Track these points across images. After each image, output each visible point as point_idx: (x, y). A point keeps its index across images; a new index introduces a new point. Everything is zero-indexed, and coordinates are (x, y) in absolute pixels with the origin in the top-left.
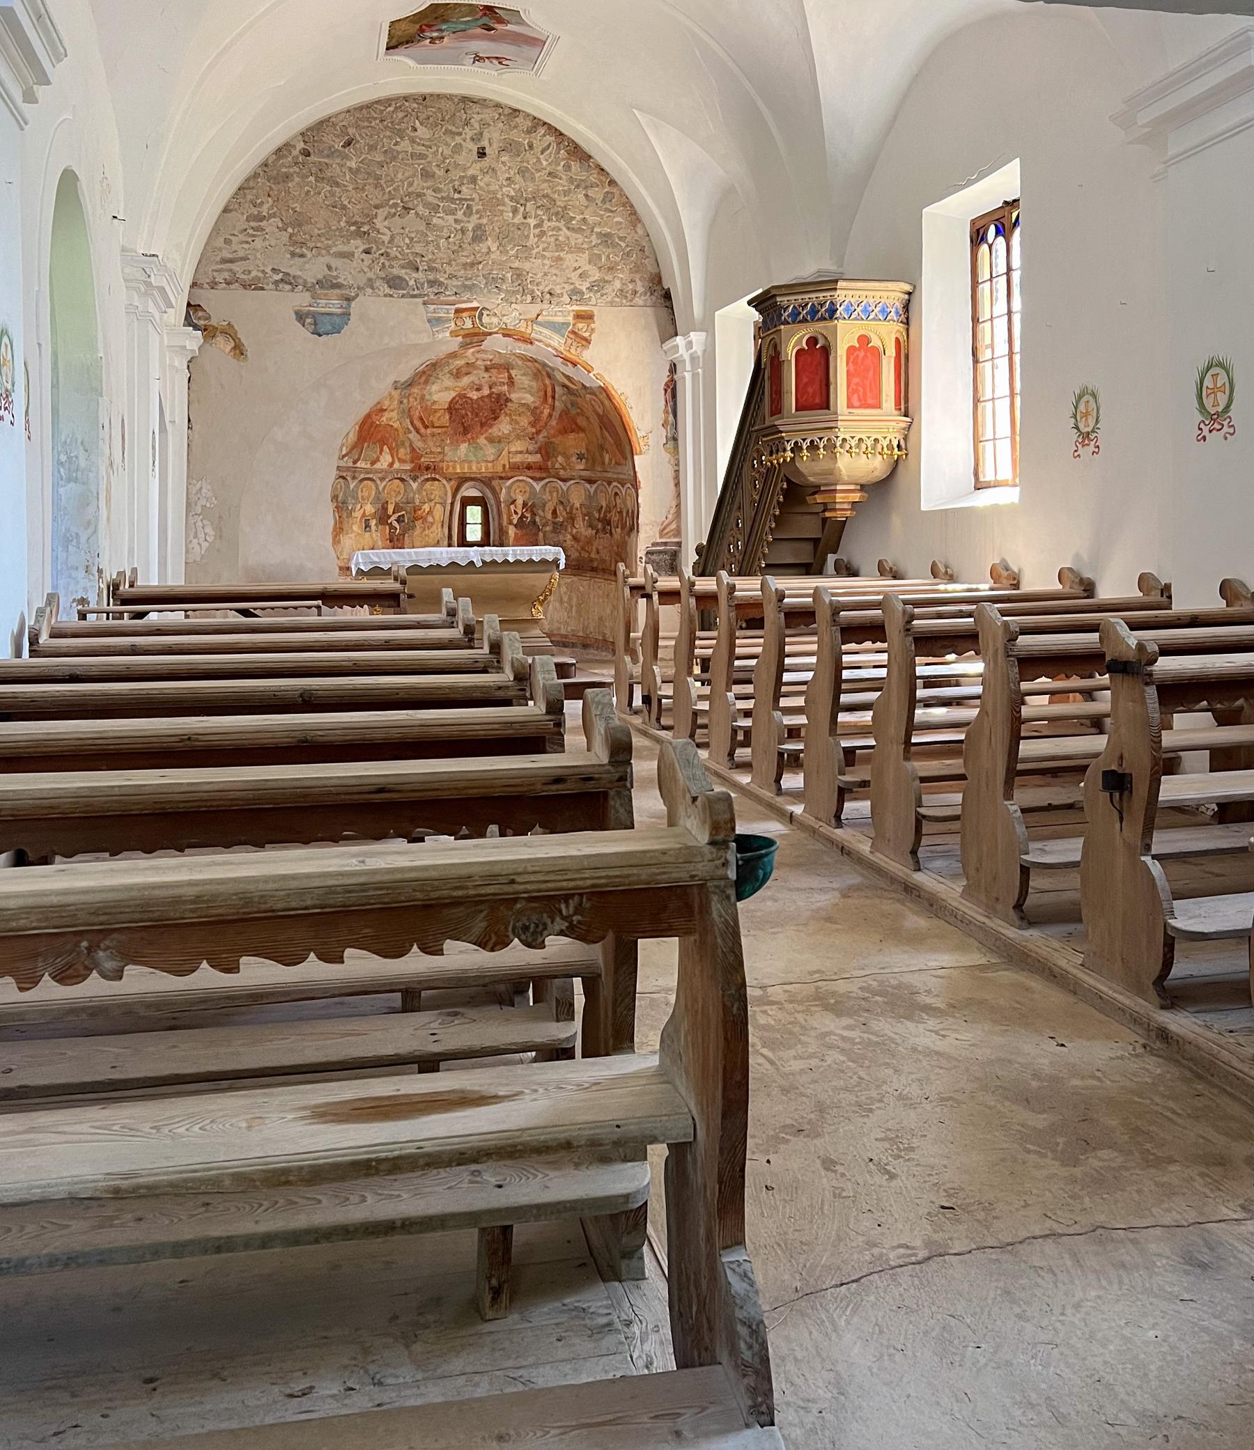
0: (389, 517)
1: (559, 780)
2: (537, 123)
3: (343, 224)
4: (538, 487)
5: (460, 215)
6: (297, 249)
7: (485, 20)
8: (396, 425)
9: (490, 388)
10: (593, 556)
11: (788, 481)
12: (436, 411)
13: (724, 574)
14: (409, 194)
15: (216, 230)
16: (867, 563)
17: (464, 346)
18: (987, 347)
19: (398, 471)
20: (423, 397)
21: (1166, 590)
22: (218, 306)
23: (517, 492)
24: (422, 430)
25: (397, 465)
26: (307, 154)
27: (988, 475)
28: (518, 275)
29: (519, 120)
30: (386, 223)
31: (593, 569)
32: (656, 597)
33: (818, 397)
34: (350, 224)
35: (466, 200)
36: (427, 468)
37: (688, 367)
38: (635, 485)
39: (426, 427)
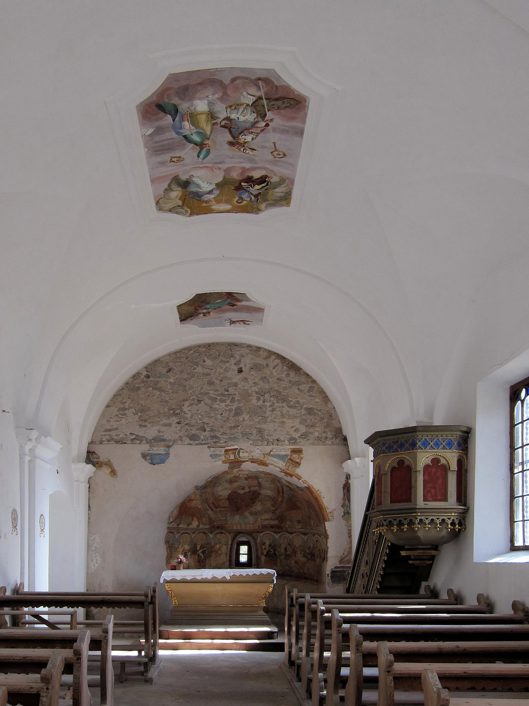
0: (198, 551)
2: (271, 353)
3: (166, 410)
4: (277, 536)
5: (228, 402)
6: (143, 422)
7: (229, 301)
8: (200, 507)
9: (249, 488)
10: (306, 571)
12: (221, 500)
14: (201, 394)
15: (103, 415)
17: (230, 468)
19: (202, 529)
20: (213, 493)
22: (104, 452)
23: (266, 539)
24: (215, 509)
25: (201, 526)
26: (148, 377)
27: (519, 543)
28: (260, 431)
29: (261, 352)
30: (189, 408)
31: (306, 578)
34: (170, 410)
35: (230, 395)
36: (218, 528)
38: (326, 537)
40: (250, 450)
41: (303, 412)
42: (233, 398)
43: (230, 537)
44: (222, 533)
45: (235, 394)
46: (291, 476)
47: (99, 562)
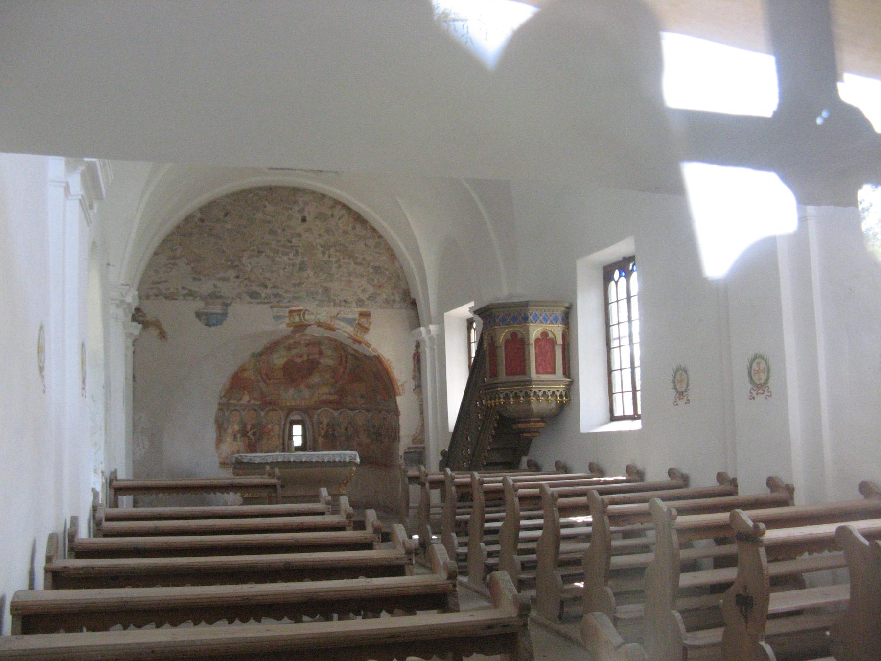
1: (490, 627)
2: (337, 203)
3: (223, 261)
4: (336, 414)
5: (291, 255)
11: (500, 415)
15: (150, 265)
16: (548, 464)
17: (294, 332)
18: (615, 339)
21: (734, 482)
22: (152, 310)
23: (325, 416)
26: (202, 220)
27: (618, 412)
32: (427, 485)
33: (518, 363)
34: (226, 261)
36: (270, 403)
37: (428, 344)
38: (397, 413)
40: (318, 313)
41: (370, 270)
42: (296, 250)
43: (283, 415)
46: (360, 343)
47: (147, 447)
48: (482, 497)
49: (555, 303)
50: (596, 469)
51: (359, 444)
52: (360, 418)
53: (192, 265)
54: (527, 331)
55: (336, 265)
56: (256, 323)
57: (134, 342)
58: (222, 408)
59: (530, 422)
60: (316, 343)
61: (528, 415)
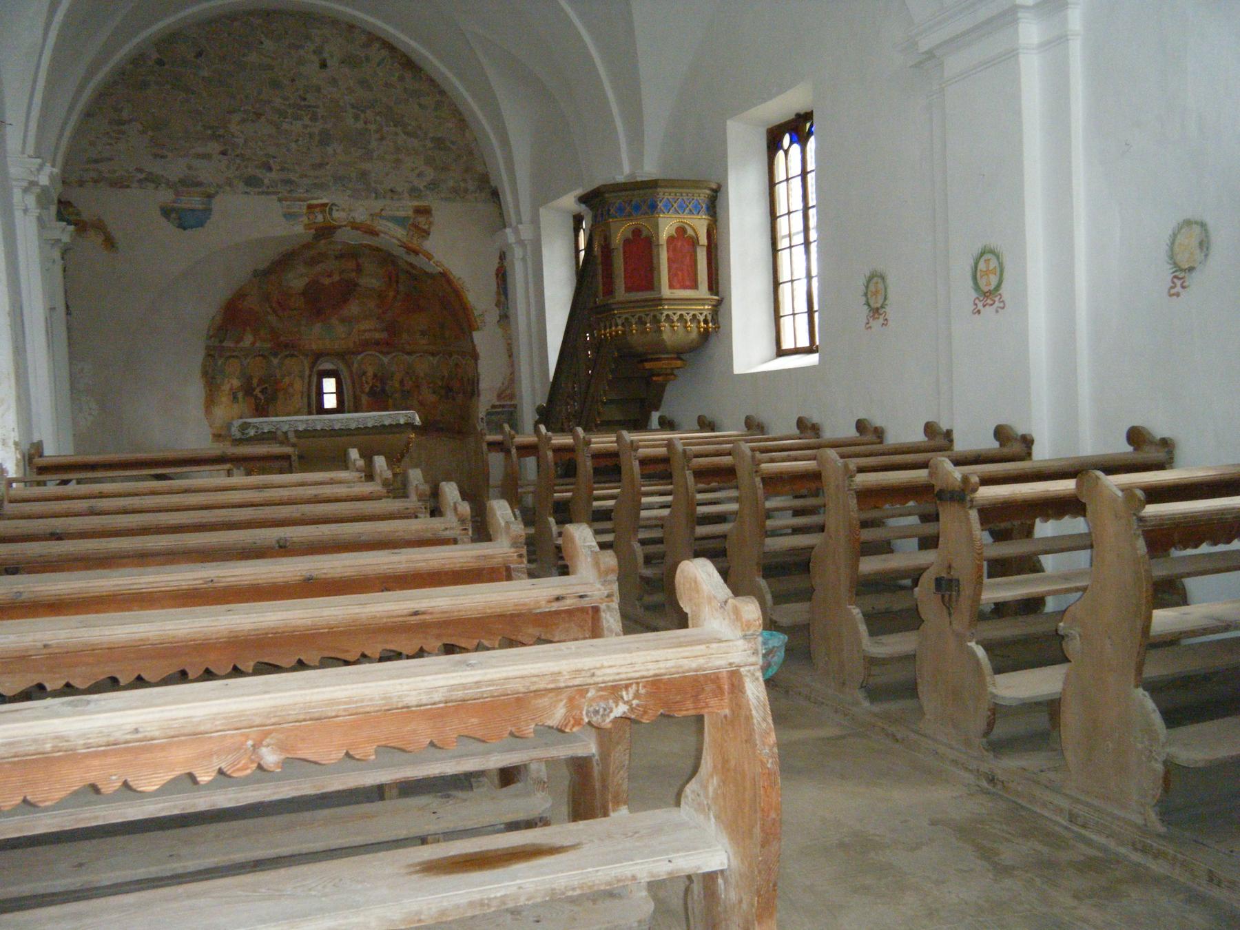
0: (254, 390)
2: (373, 38)
3: (199, 128)
4: (385, 360)
5: (306, 121)
9: (340, 274)
13: (580, 430)
15: (79, 132)
18: (784, 237)
21: (948, 434)
22: (90, 203)
23: (369, 363)
26: (160, 63)
27: (787, 344)
32: (514, 451)
33: (644, 277)
36: (286, 346)
38: (475, 357)
39: (284, 310)
40: (350, 209)
44: (292, 355)
45: (317, 107)
46: (416, 253)
48: (589, 463)
49: (696, 184)
50: (753, 425)
51: (421, 403)
52: (423, 366)
53: (150, 133)
54: (657, 226)
55: (377, 136)
56: (254, 223)
57: (65, 252)
58: (210, 355)
59: (658, 359)
60: (351, 254)
61: (659, 349)
